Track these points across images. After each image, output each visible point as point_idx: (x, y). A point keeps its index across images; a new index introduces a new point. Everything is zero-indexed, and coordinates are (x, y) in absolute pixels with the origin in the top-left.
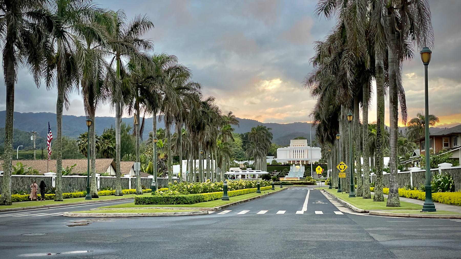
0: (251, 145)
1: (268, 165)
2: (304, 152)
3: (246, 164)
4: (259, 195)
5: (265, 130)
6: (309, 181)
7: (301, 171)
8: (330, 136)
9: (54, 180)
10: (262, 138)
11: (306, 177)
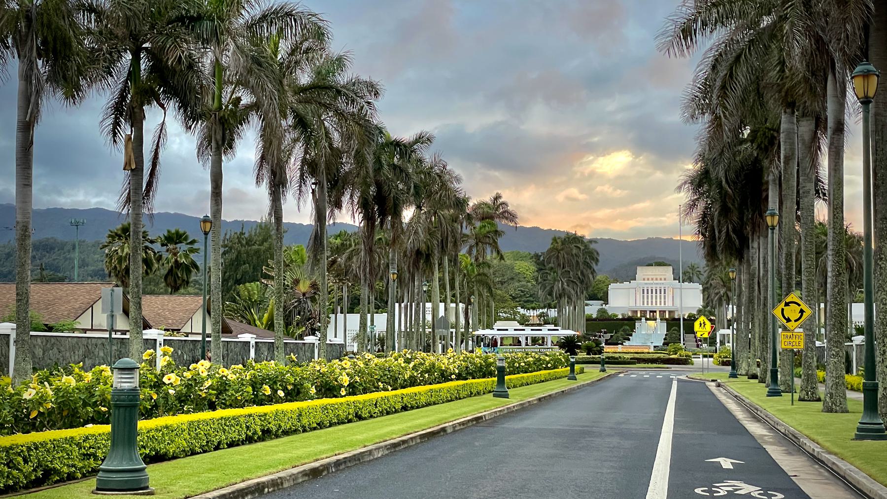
0: (550, 274)
1: (589, 319)
2: (665, 293)
3: (544, 316)
4: (573, 384)
5: (582, 242)
6: (676, 354)
7: (659, 333)
8: (733, 236)
9: (160, 344)
10: (573, 258)
11: (668, 345)
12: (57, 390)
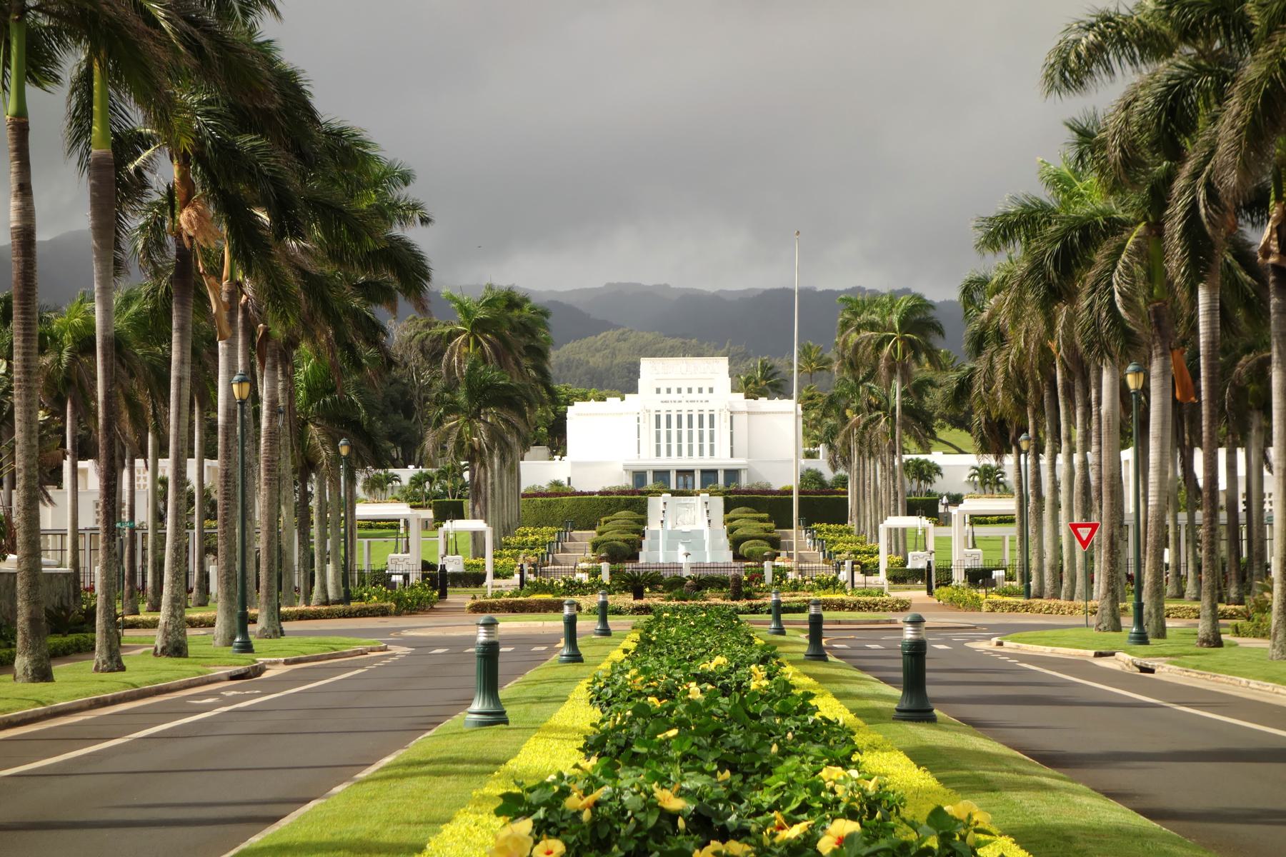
2: (712, 424)
12: (1251, 381)
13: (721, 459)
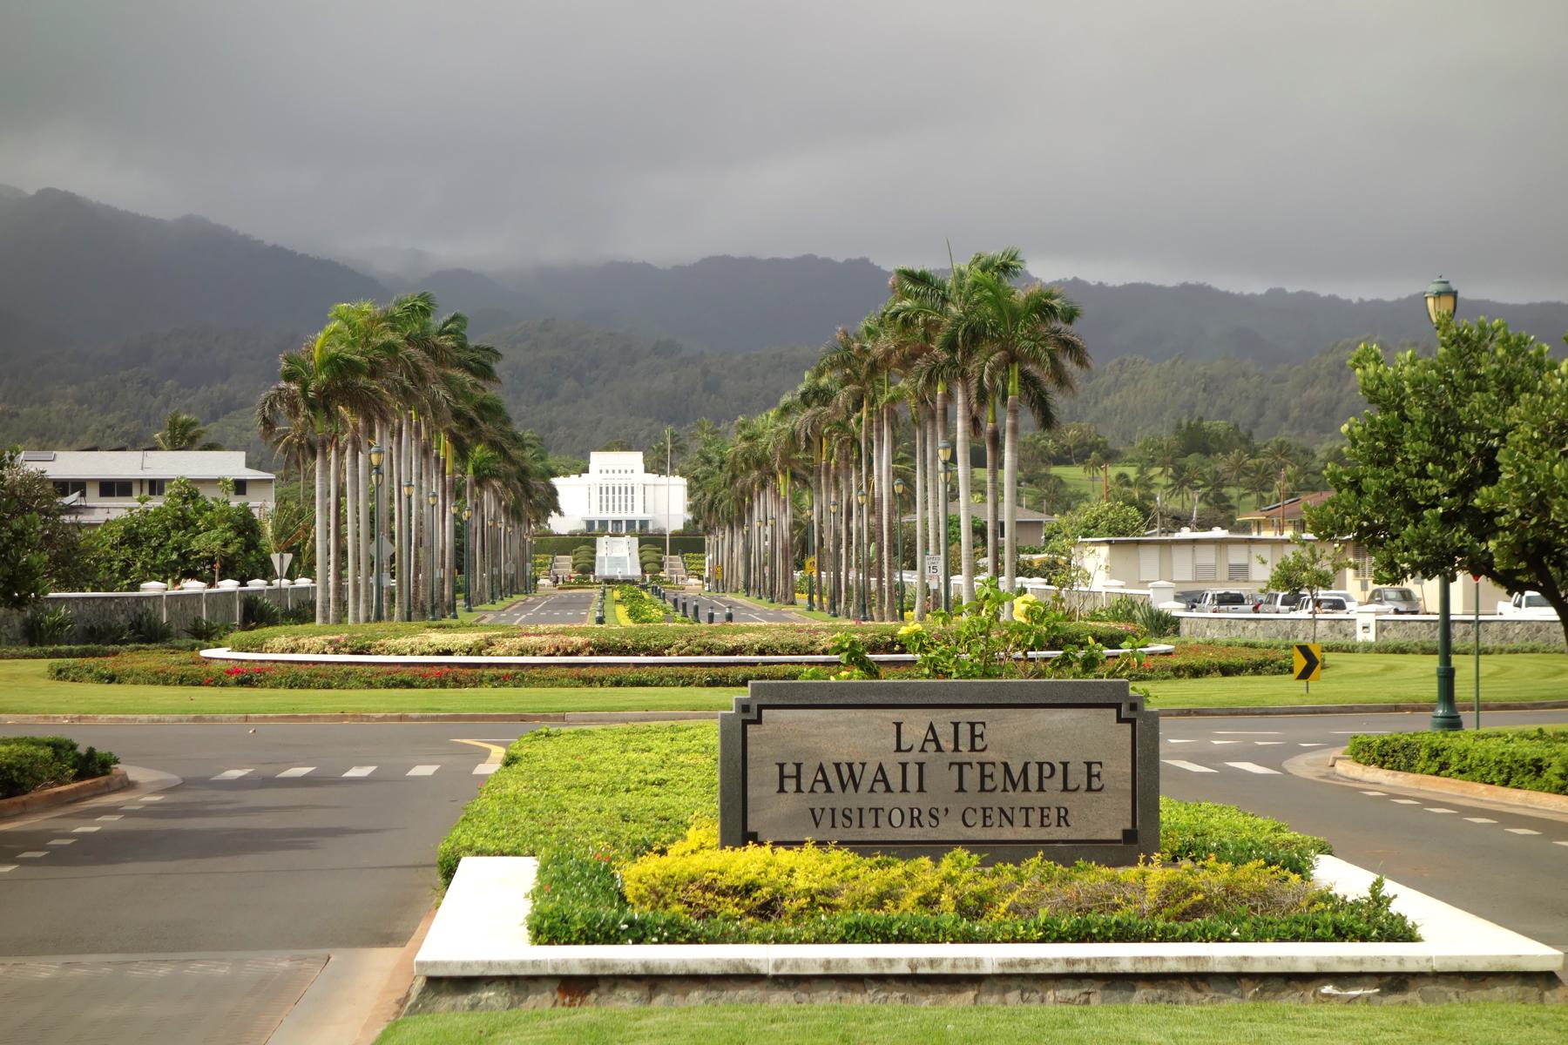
2: (633, 493)
13: (638, 514)
